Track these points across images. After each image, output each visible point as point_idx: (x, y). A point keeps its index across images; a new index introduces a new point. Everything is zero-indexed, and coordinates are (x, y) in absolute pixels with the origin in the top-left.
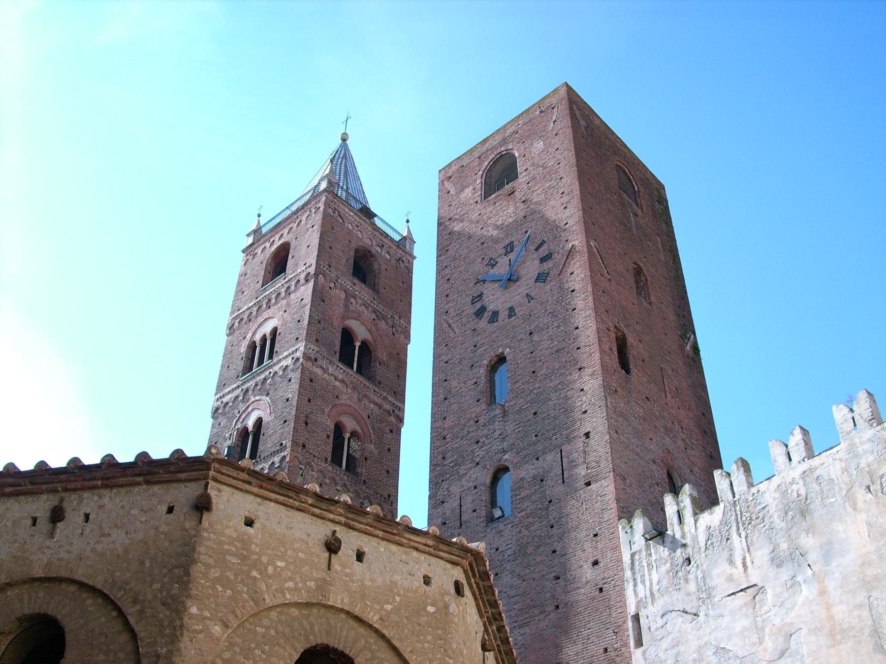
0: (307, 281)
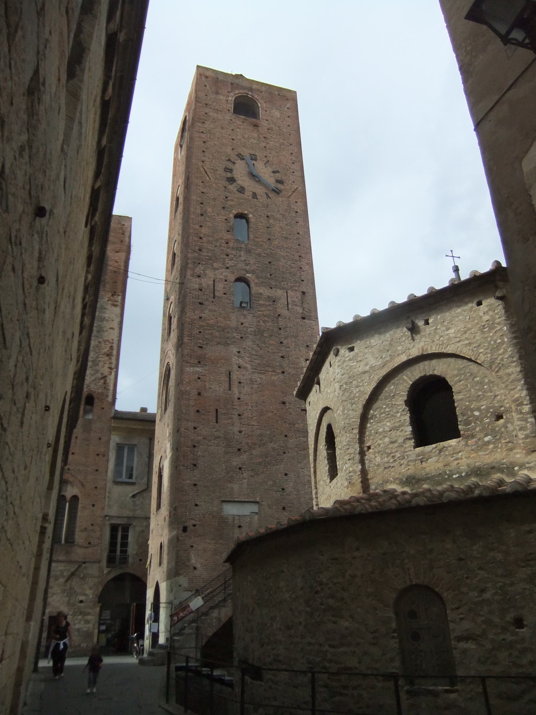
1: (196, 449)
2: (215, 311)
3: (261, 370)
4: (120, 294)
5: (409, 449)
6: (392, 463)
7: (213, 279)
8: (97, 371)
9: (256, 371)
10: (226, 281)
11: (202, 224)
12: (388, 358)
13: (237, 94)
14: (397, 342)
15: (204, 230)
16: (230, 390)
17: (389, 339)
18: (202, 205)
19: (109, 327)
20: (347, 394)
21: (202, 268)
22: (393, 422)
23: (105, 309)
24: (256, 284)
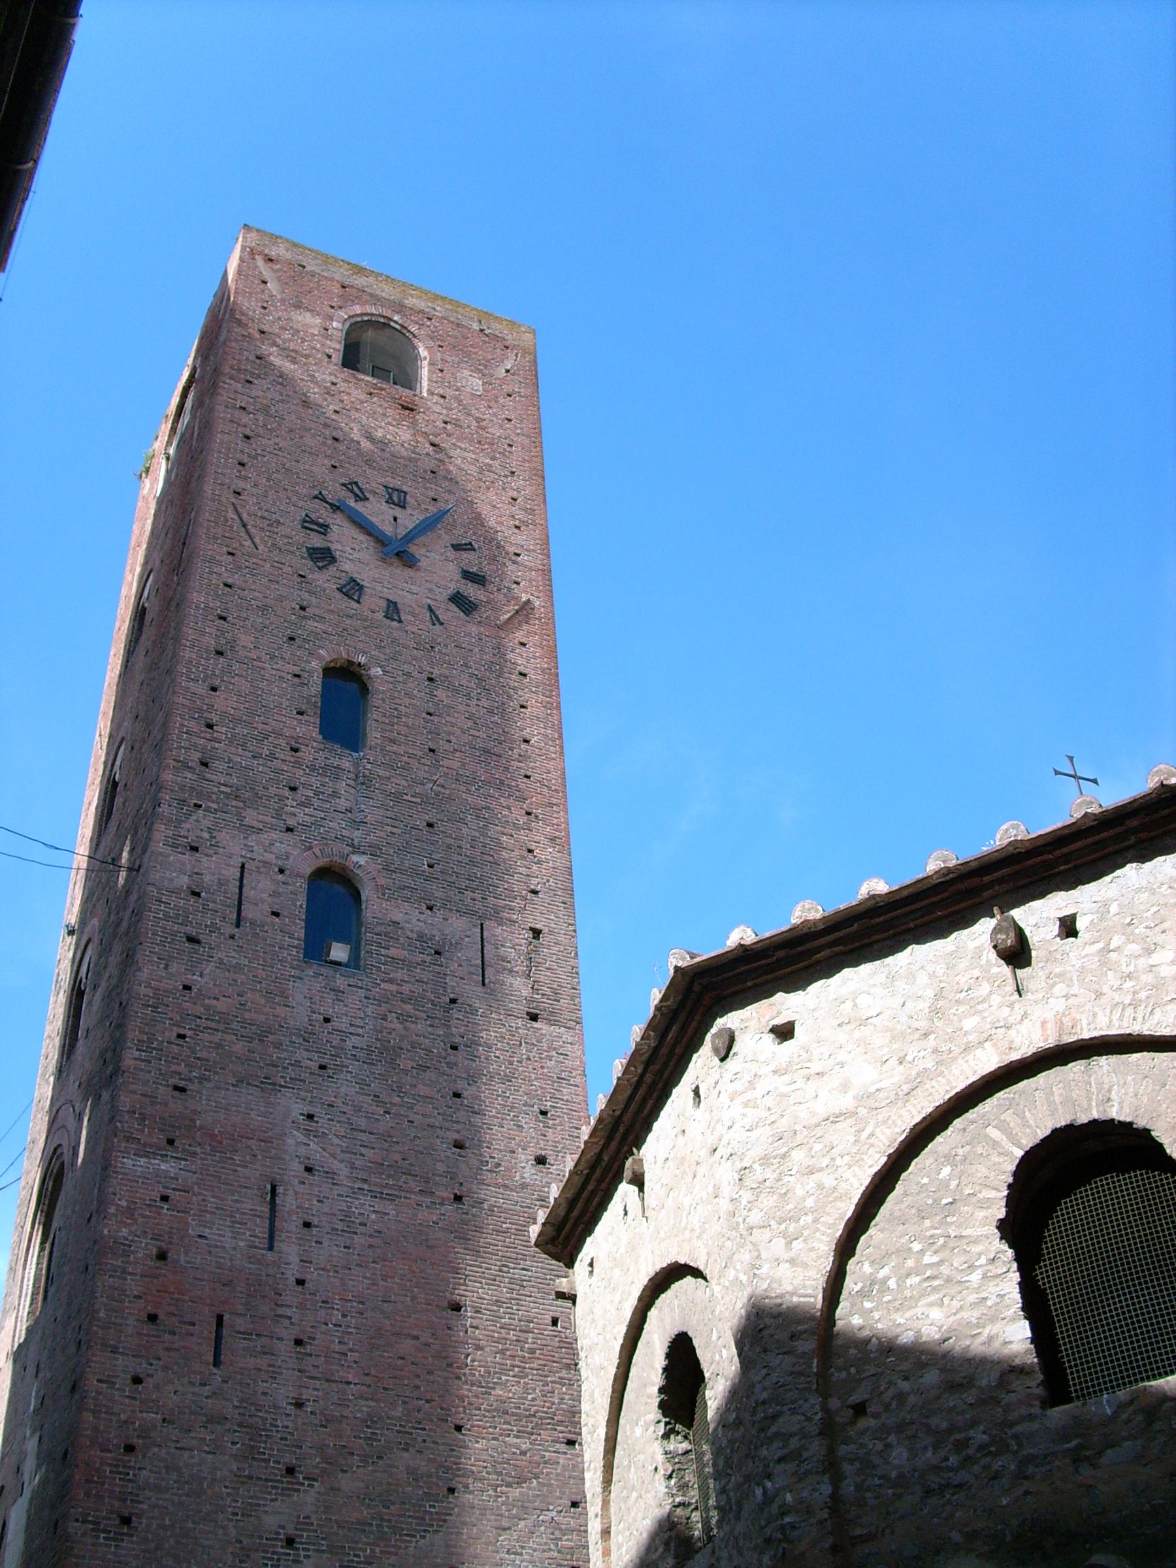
1: (131, 1459)
2: (238, 968)
3: (382, 1186)
5: (1023, 1411)
6: (955, 1470)
7: (241, 860)
9: (366, 1187)
10: (281, 871)
11: (217, 683)
12: (930, 1064)
13: (357, 315)
14: (958, 1002)
15: (219, 701)
17: (930, 993)
18: (222, 622)
20: (767, 1202)
21: (206, 823)
22: (956, 1304)
24: (382, 890)
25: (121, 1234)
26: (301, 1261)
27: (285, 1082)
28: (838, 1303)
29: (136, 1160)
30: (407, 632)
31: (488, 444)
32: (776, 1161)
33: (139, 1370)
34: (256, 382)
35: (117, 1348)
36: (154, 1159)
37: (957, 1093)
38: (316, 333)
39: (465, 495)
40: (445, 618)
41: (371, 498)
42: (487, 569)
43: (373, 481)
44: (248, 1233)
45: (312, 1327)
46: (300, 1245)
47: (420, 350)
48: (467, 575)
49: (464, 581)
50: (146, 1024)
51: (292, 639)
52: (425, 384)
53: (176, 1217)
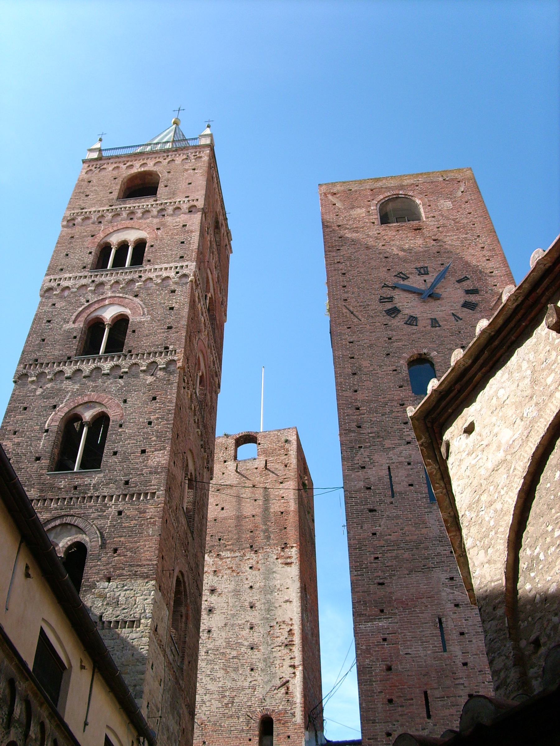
0: (190, 212)
2: (397, 517)
4: (294, 545)
7: (387, 465)
8: (273, 675)
13: (382, 199)
15: (360, 396)
16: (445, 650)
17: (529, 372)
18: (353, 360)
19: (282, 600)
23: (274, 572)
25: (366, 663)
26: (463, 653)
27: (434, 565)
28: (518, 579)
29: (366, 625)
30: (444, 330)
31: (462, 228)
32: (474, 506)
33: (388, 729)
34: (341, 248)
35: (375, 720)
36: (375, 622)
37: (550, 424)
38: (364, 215)
39: (457, 256)
40: (462, 316)
41: (410, 276)
42: (478, 285)
43: (408, 268)
44: (431, 646)
45: (476, 686)
46: (460, 645)
47: (417, 201)
48: (468, 292)
49: (468, 295)
50: (358, 558)
51: (388, 354)
52: (423, 215)
53: (392, 647)
